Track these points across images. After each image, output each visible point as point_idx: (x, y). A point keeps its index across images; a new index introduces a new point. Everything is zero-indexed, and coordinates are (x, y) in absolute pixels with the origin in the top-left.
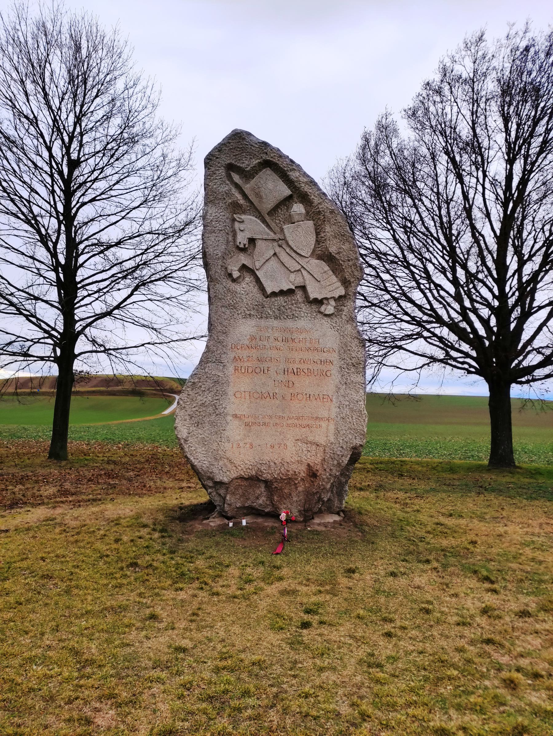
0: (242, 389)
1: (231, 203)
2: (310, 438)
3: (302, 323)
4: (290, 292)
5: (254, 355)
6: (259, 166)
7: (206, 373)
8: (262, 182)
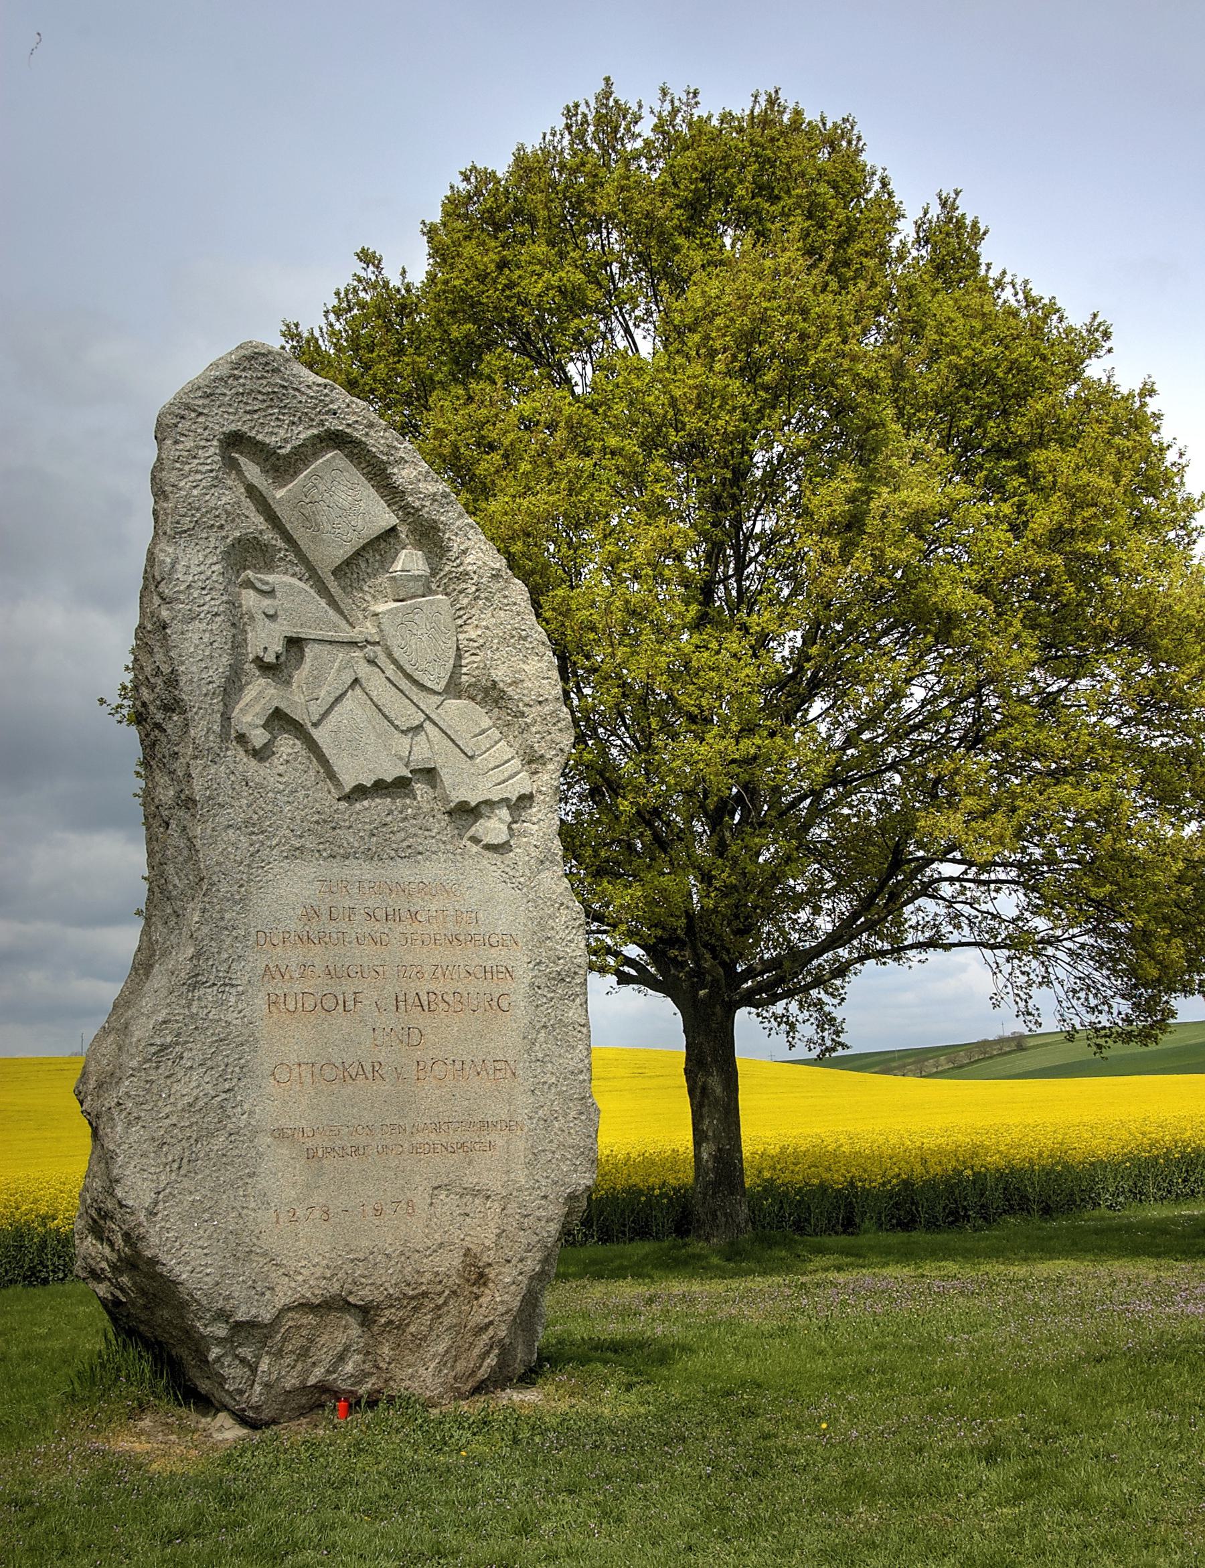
0: (293, 1058)
1: (239, 540)
2: (470, 1181)
3: (432, 870)
4: (401, 785)
5: (317, 961)
6: (313, 445)
7: (192, 1016)
8: (322, 488)
